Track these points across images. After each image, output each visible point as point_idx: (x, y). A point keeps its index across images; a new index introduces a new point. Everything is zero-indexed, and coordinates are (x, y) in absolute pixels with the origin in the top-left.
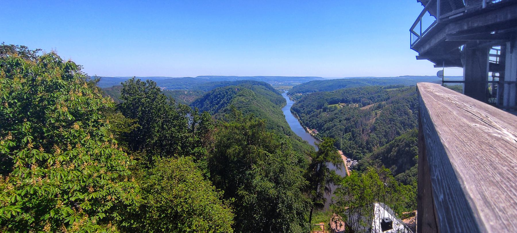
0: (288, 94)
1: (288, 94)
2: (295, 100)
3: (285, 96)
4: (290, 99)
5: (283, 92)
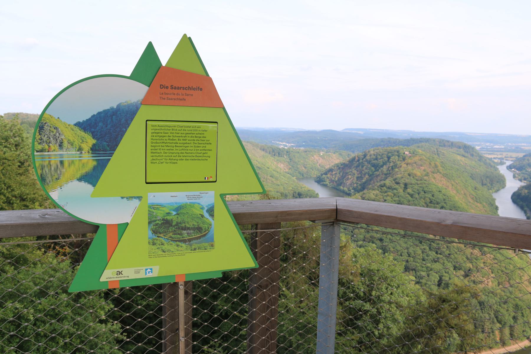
0: (509, 168)
1: (509, 168)
2: (525, 179)
3: (503, 170)
4: (514, 177)
5: (502, 163)
